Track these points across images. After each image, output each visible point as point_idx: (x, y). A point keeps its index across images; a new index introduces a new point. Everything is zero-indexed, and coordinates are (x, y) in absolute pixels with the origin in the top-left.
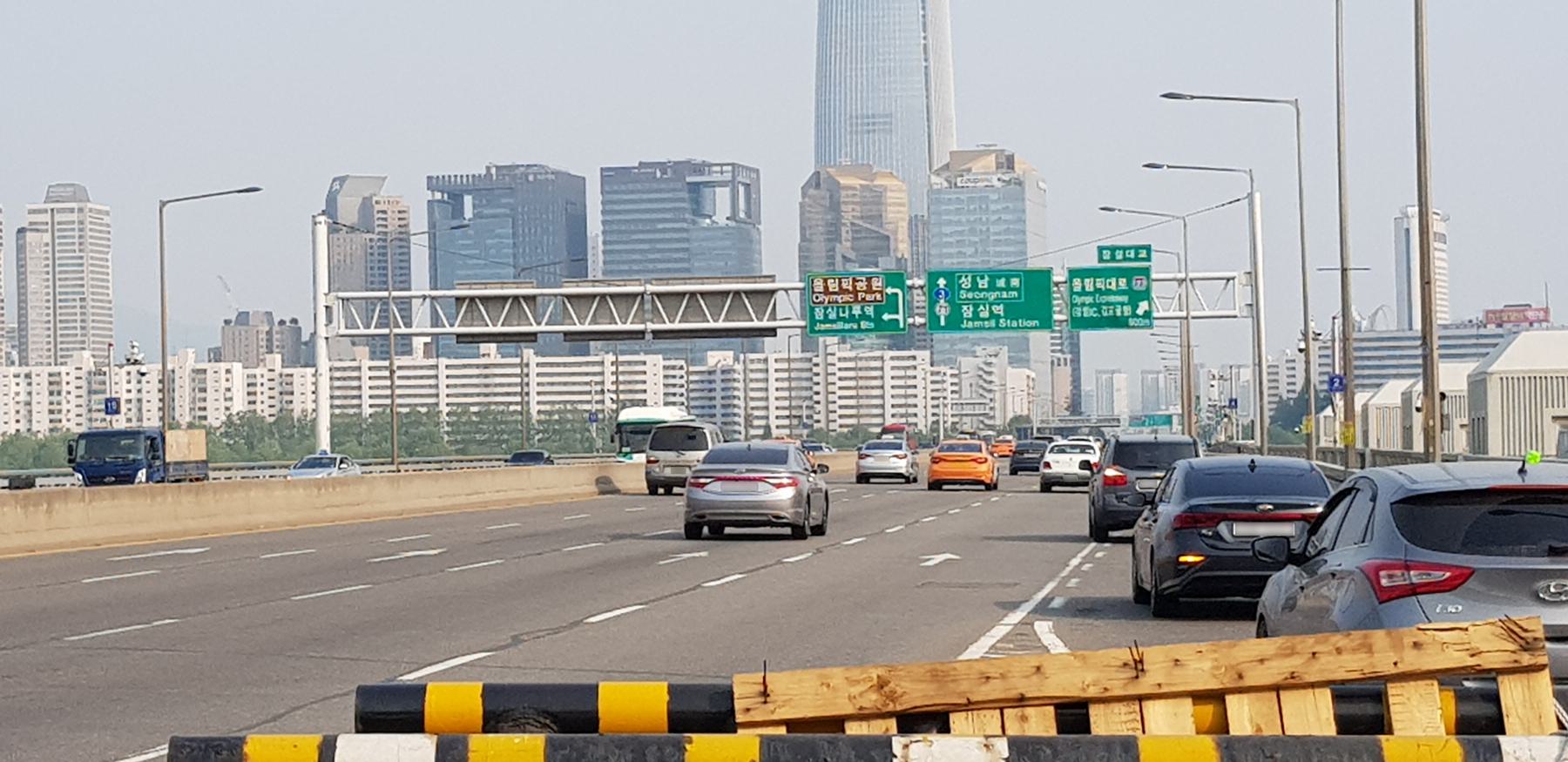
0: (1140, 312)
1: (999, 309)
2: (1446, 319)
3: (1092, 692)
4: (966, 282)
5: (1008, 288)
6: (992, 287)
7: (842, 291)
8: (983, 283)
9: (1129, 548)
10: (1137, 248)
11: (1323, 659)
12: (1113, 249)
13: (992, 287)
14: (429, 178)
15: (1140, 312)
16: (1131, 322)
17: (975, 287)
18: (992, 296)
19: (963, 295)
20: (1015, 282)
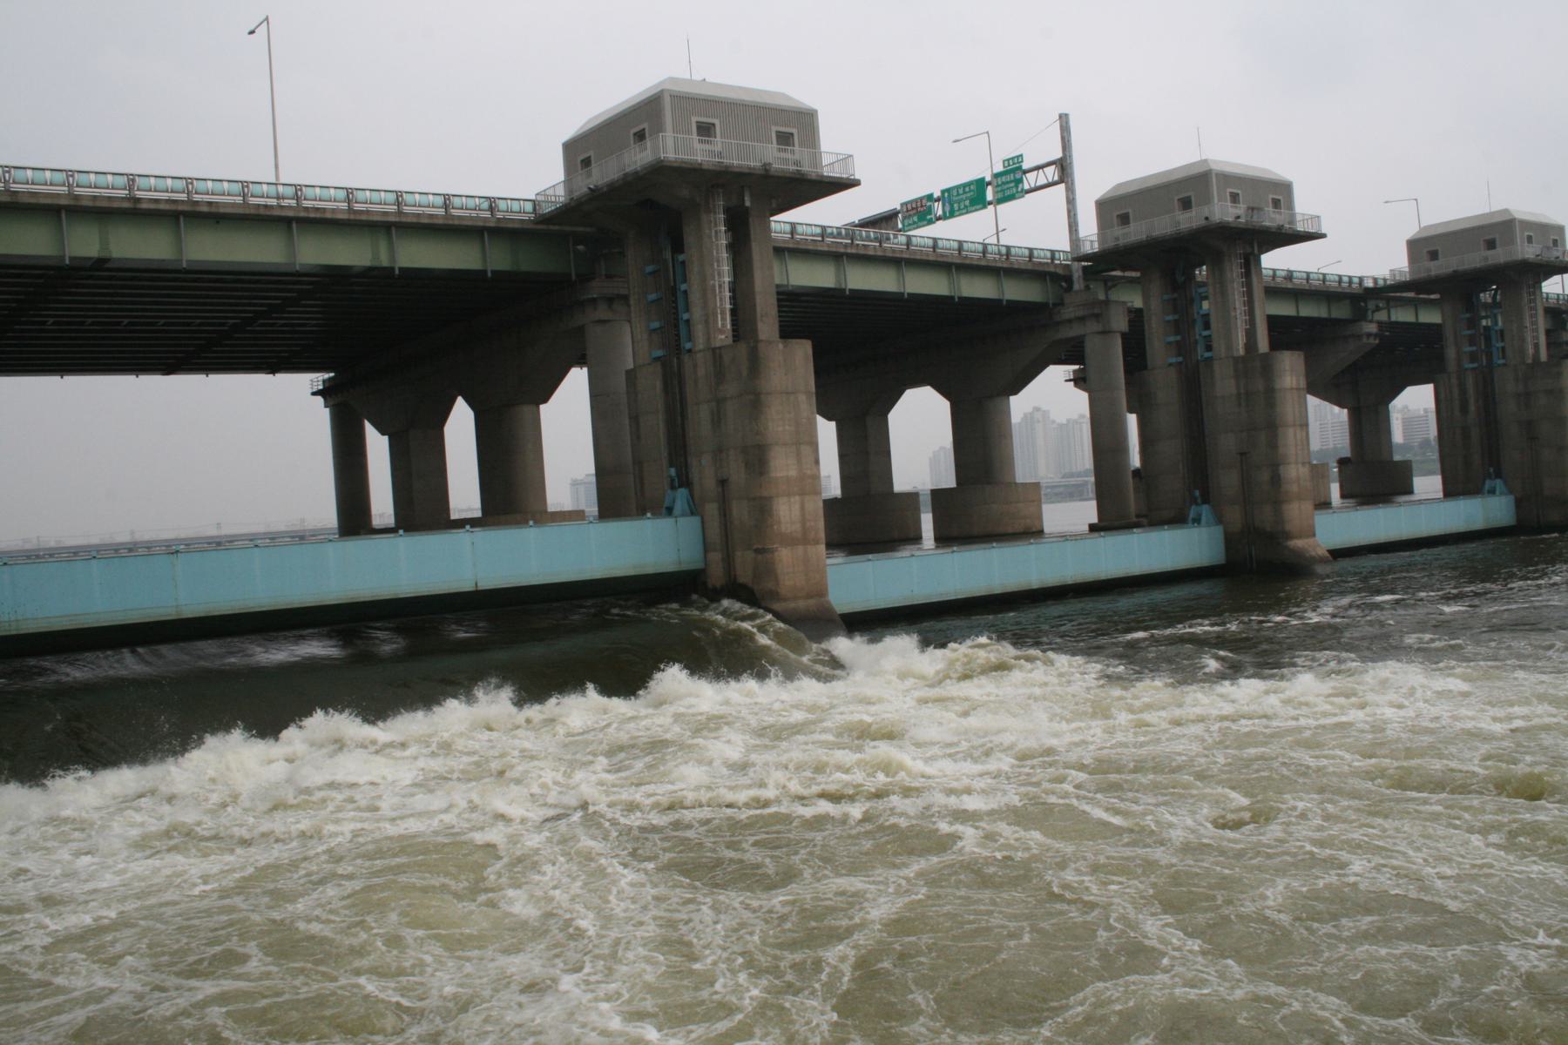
0: (1020, 189)
1: (967, 203)
2: (667, 609)
3: (696, 487)
4: (955, 193)
5: (970, 191)
6: (965, 192)
7: (913, 209)
8: (961, 191)
9: (324, 510)
10: (1018, 157)
11: (1176, 968)
12: (1008, 160)
13: (965, 192)
14: (1021, 155)
15: (1020, 189)
16: (1017, 195)
17: (958, 195)
18: (964, 196)
19: (955, 199)
20: (972, 187)
